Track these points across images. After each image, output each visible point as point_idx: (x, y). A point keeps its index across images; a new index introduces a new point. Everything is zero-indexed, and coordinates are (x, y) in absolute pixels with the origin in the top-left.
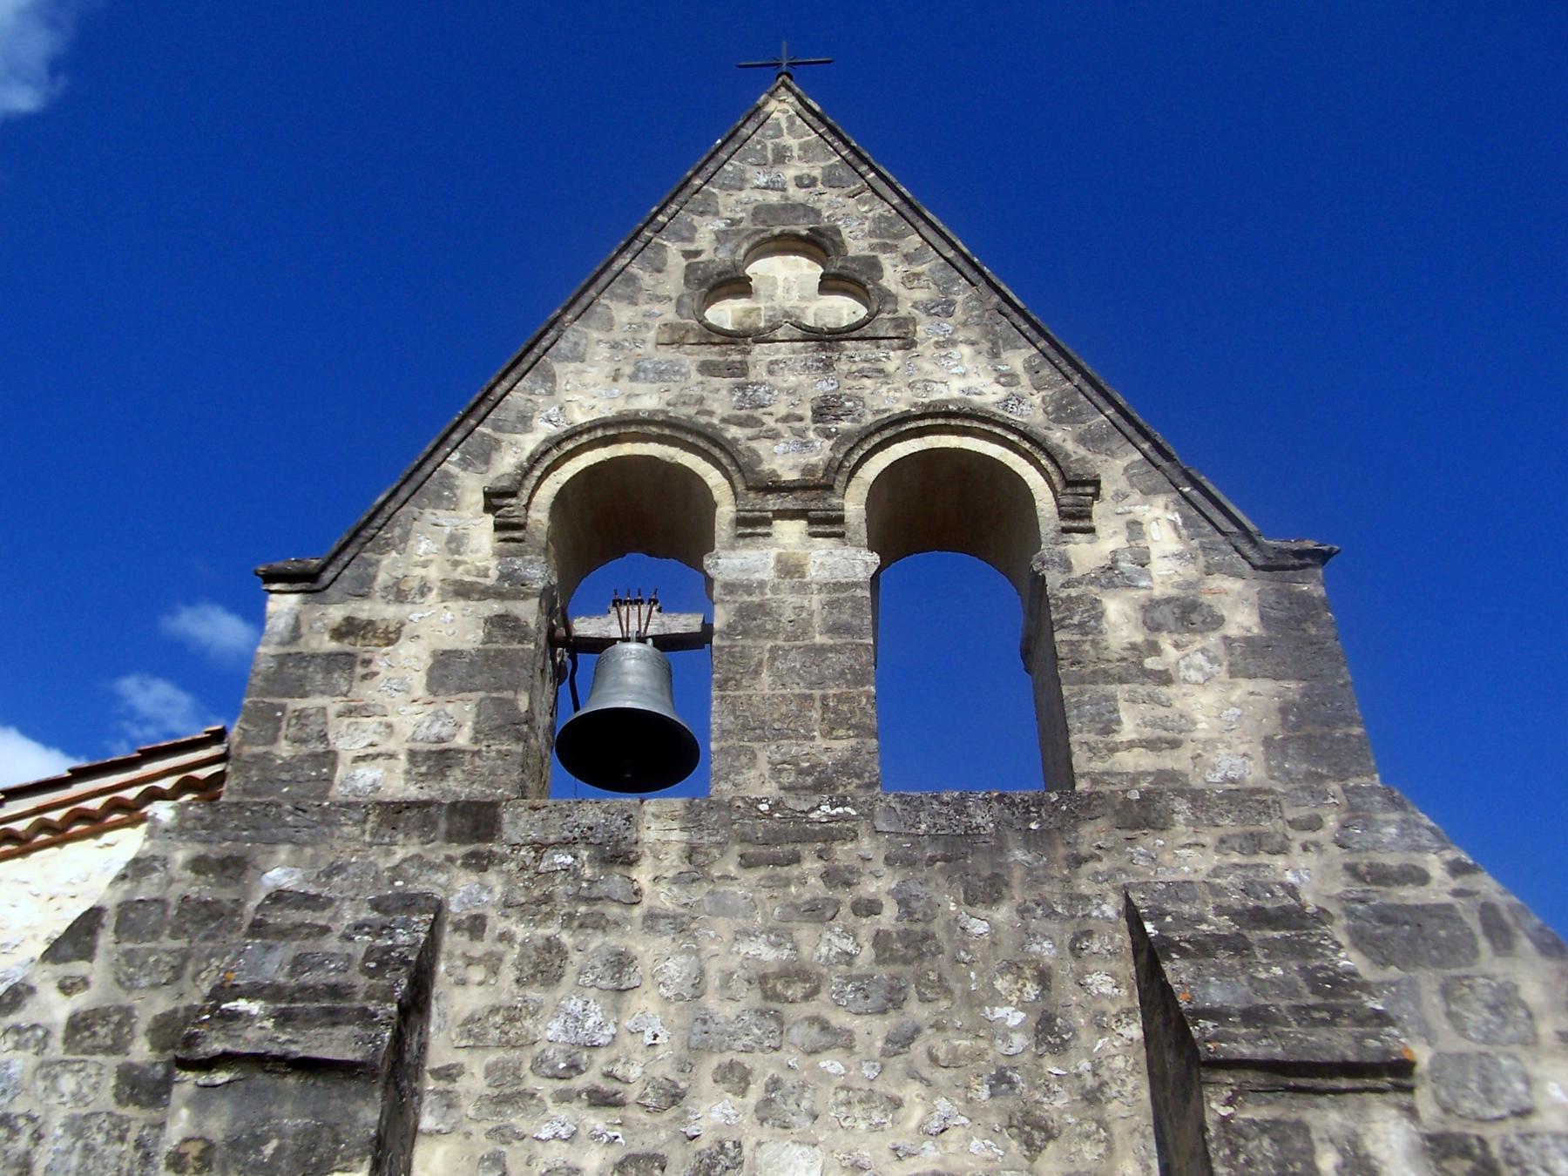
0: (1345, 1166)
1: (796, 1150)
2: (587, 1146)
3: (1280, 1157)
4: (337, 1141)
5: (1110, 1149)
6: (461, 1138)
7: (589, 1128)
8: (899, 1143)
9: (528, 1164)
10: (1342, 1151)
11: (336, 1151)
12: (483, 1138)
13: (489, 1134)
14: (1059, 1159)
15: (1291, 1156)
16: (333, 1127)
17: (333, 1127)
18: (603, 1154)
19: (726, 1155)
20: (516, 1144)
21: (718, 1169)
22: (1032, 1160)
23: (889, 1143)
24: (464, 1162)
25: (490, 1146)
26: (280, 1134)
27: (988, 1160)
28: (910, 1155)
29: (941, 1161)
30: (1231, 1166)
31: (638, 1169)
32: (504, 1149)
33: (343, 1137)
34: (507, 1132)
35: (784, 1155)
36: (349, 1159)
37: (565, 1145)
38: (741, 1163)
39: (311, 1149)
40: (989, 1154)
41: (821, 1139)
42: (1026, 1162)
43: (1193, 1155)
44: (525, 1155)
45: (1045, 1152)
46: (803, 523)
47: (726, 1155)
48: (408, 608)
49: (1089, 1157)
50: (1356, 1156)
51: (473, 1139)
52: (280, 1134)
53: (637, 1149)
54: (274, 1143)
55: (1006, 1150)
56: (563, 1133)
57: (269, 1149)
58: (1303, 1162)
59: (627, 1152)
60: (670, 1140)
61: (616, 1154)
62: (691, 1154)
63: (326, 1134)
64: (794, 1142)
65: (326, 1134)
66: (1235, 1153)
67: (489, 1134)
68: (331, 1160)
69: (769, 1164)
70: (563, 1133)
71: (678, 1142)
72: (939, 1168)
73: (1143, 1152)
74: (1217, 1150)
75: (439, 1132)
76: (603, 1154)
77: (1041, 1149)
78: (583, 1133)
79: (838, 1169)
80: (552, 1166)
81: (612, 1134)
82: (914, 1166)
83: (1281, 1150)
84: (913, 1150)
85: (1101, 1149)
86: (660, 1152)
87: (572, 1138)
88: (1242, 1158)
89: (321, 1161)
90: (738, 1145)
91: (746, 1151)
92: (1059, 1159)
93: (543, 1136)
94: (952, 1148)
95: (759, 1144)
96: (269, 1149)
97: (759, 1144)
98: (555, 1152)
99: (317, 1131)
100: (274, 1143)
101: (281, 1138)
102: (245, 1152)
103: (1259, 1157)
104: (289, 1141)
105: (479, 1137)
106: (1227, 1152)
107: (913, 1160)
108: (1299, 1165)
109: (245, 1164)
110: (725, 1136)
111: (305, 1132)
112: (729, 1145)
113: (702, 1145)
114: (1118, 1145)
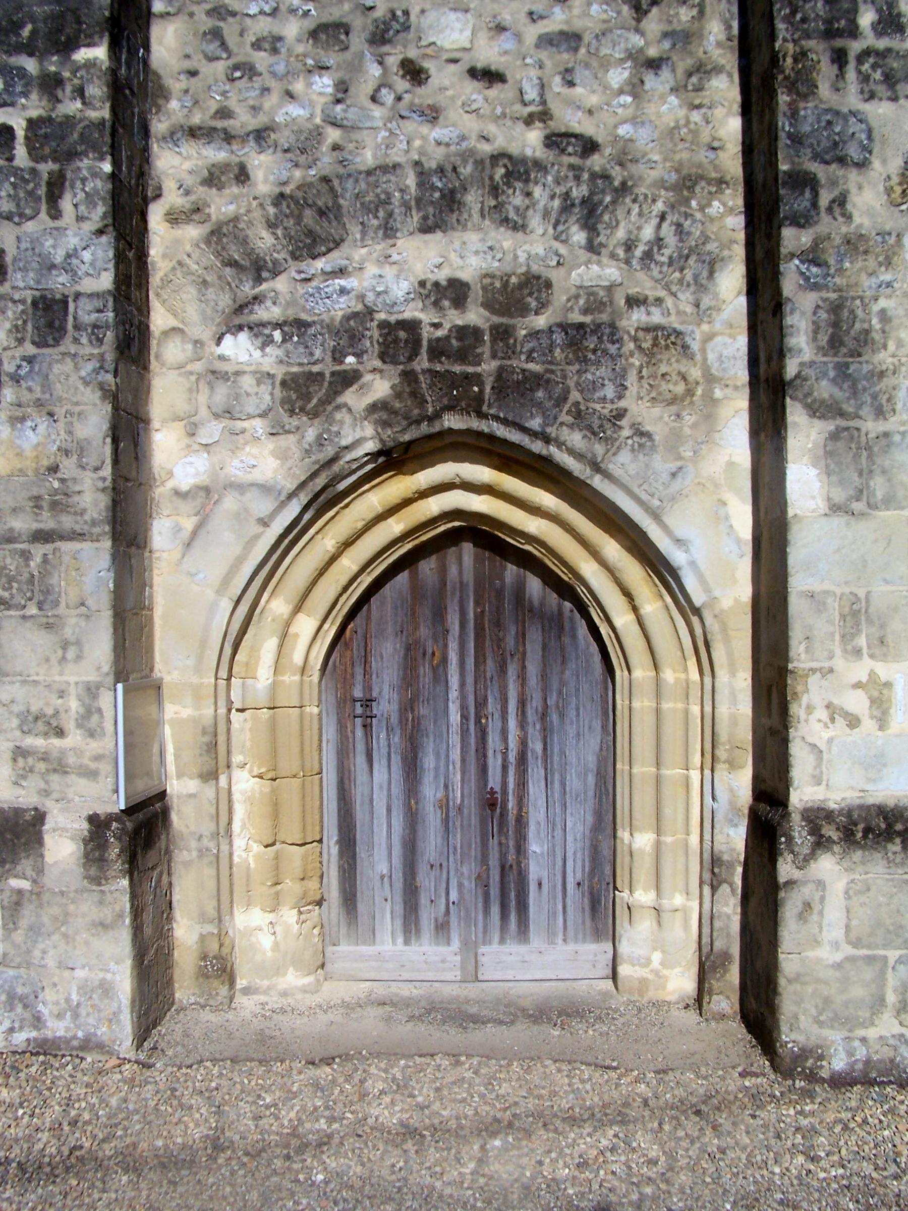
0: (879, 22)
1: (453, 16)
2: (287, 19)
3: (829, 15)
4: (79, 23)
5: (702, 12)
6: (186, 18)
7: (287, 4)
8: (534, 8)
9: (241, 35)
10: (879, 11)
11: (80, 31)
12: (203, 16)
13: (209, 13)
14: (660, 20)
15: (837, 15)
16: (75, 12)
17: (75, 12)
18: (299, 24)
19: (397, 21)
20: (230, 20)
21: (391, 33)
22: (639, 21)
23: (526, 9)
24: (191, 37)
25: (210, 23)
26: (33, 19)
27: (604, 21)
28: (542, 17)
29: (567, 22)
30: (789, 23)
31: (328, 35)
32: (222, 24)
33: (84, 19)
34: (223, 11)
35: (443, 20)
36: (91, 36)
37: (269, 19)
38: (409, 27)
39: (60, 31)
40: (605, 16)
41: (472, 6)
42: (634, 23)
43: (763, 15)
44: (237, 28)
45: (650, 15)
46: (228, 335)
47: (397, 21)
48: (19, 466)
49: (684, 18)
50: (890, 14)
51: (196, 18)
52: (33, 19)
53: (326, 18)
54: (29, 27)
55: (619, 13)
56: (267, 9)
57: (26, 31)
58: (848, 20)
59: (319, 21)
60: (352, 11)
61: (309, 24)
62: (369, 21)
63: (69, 17)
64: (451, 9)
65: (69, 17)
66: (793, 13)
67: (209, 13)
68: (77, 38)
69: (431, 27)
70: (267, 9)
71: (358, 13)
72: (564, 27)
73: (727, 15)
74: (780, 10)
75: (168, 14)
76: (299, 24)
77: (646, 12)
78: (283, 8)
79: (486, 30)
80: (260, 35)
81: (306, 8)
82: (545, 27)
83: (830, 10)
84: (545, 13)
85: (694, 12)
86: (344, 20)
87: (274, 12)
88: (799, 16)
89: (69, 39)
90: (406, 13)
91: (413, 18)
92: (660, 20)
93: (251, 12)
94: (576, 12)
95: (423, 11)
96: (26, 31)
97: (423, 11)
98: (262, 24)
99: (62, 15)
100: (29, 27)
101: (34, 22)
102: (7, 35)
103: (813, 15)
104: (41, 25)
105: (201, 16)
106: (788, 11)
107: (545, 22)
108: (843, 22)
109: (9, 45)
110: (395, 6)
111: (52, 17)
112: (399, 13)
113: (379, 13)
114: (708, 9)
